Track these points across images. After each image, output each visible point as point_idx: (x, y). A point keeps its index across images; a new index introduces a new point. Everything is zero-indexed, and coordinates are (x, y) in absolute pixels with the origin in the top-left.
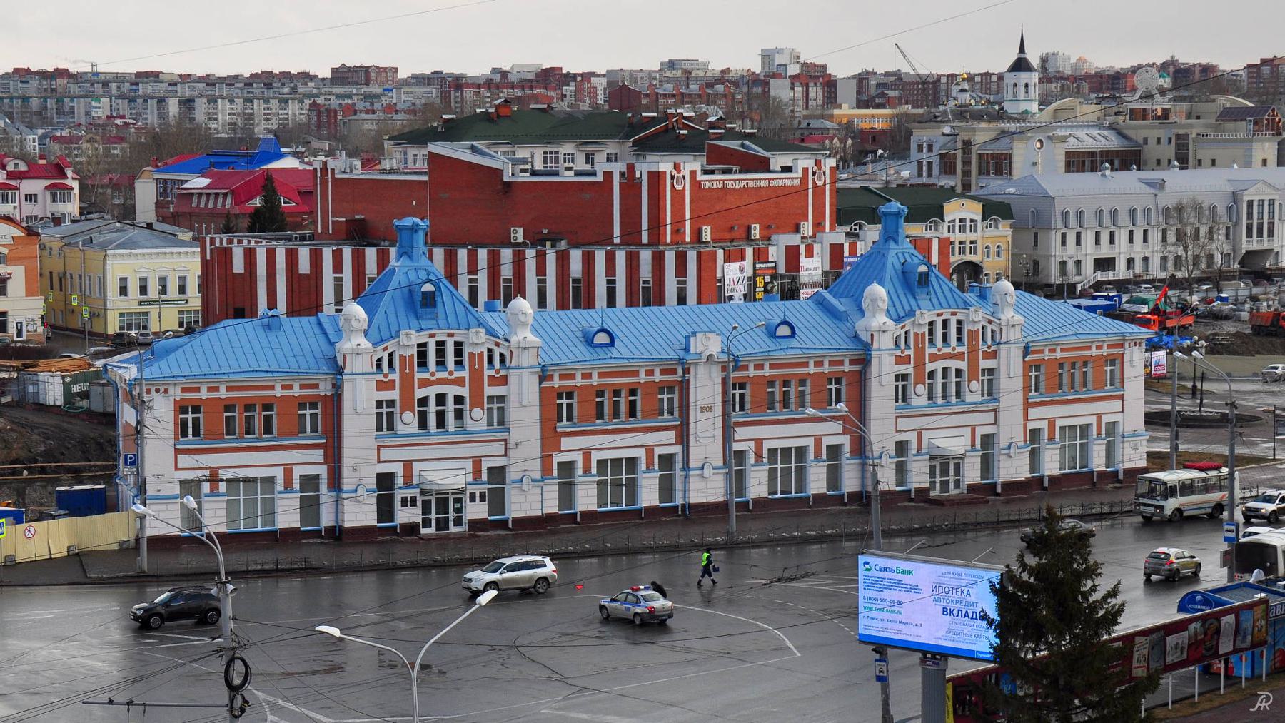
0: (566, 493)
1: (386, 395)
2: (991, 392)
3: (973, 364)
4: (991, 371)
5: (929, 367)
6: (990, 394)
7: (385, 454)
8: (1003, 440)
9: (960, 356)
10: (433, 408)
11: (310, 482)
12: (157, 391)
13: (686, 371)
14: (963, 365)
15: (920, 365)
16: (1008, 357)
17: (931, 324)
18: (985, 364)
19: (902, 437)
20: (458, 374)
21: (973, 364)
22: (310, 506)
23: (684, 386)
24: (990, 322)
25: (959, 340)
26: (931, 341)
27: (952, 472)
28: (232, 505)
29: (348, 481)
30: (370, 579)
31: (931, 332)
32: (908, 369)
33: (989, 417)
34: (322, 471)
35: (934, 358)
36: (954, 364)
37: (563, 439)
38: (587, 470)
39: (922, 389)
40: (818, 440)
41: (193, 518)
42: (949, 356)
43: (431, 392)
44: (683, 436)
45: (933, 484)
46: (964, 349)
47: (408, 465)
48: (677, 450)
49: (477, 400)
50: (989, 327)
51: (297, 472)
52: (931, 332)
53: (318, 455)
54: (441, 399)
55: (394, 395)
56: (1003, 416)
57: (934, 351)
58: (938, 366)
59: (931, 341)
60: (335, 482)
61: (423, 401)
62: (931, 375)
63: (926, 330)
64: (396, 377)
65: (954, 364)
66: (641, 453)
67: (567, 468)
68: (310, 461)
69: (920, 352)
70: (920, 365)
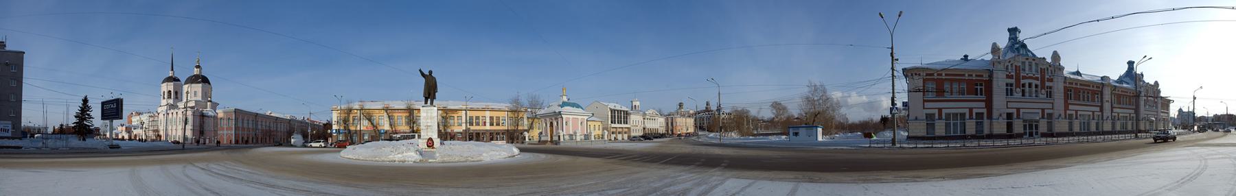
0: (1071, 124)
1: (1010, 81)
5: (1022, 81)
7: (1010, 105)
8: (1056, 115)
10: (1027, 89)
11: (980, 115)
14: (1038, 83)
15: (1018, 80)
18: (1047, 84)
19: (1010, 111)
22: (979, 125)
28: (947, 125)
29: (995, 114)
30: (565, 142)
33: (1050, 106)
34: (985, 111)
36: (1034, 82)
38: (940, 118)
40: (971, 110)
41: (670, 123)
47: (1018, 110)
49: (1043, 87)
51: (975, 111)
53: (983, 104)
54: (1030, 85)
55: (1013, 81)
58: (1027, 82)
60: (990, 116)
62: (1024, 85)
66: (967, 111)
67: (1071, 116)
68: (979, 107)
69: (1018, 75)
70: (1018, 80)
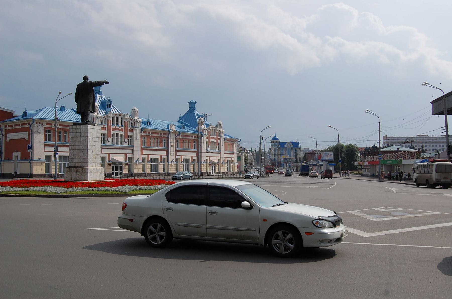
2: (131, 142)
3: (126, 133)
4: (130, 137)
5: (112, 132)
6: (130, 144)
9: (122, 130)
12: (40, 123)
13: (169, 134)
14: (123, 133)
16: (136, 133)
17: (113, 118)
18: (130, 134)
20: (121, 128)
21: (126, 133)
23: (168, 138)
24: (131, 120)
25: (121, 124)
26: (113, 124)
27: (119, 170)
31: (113, 120)
32: (105, 132)
33: (130, 151)
35: (114, 129)
36: (120, 133)
37: (144, 151)
39: (110, 139)
42: (118, 129)
43: (115, 132)
44: (167, 154)
45: (113, 173)
46: (123, 128)
48: (166, 157)
50: (131, 122)
52: (113, 120)
56: (135, 153)
57: (114, 127)
58: (115, 132)
59: (113, 124)
61: (113, 135)
63: (111, 119)
64: (106, 126)
65: (120, 133)
70: (109, 131)
